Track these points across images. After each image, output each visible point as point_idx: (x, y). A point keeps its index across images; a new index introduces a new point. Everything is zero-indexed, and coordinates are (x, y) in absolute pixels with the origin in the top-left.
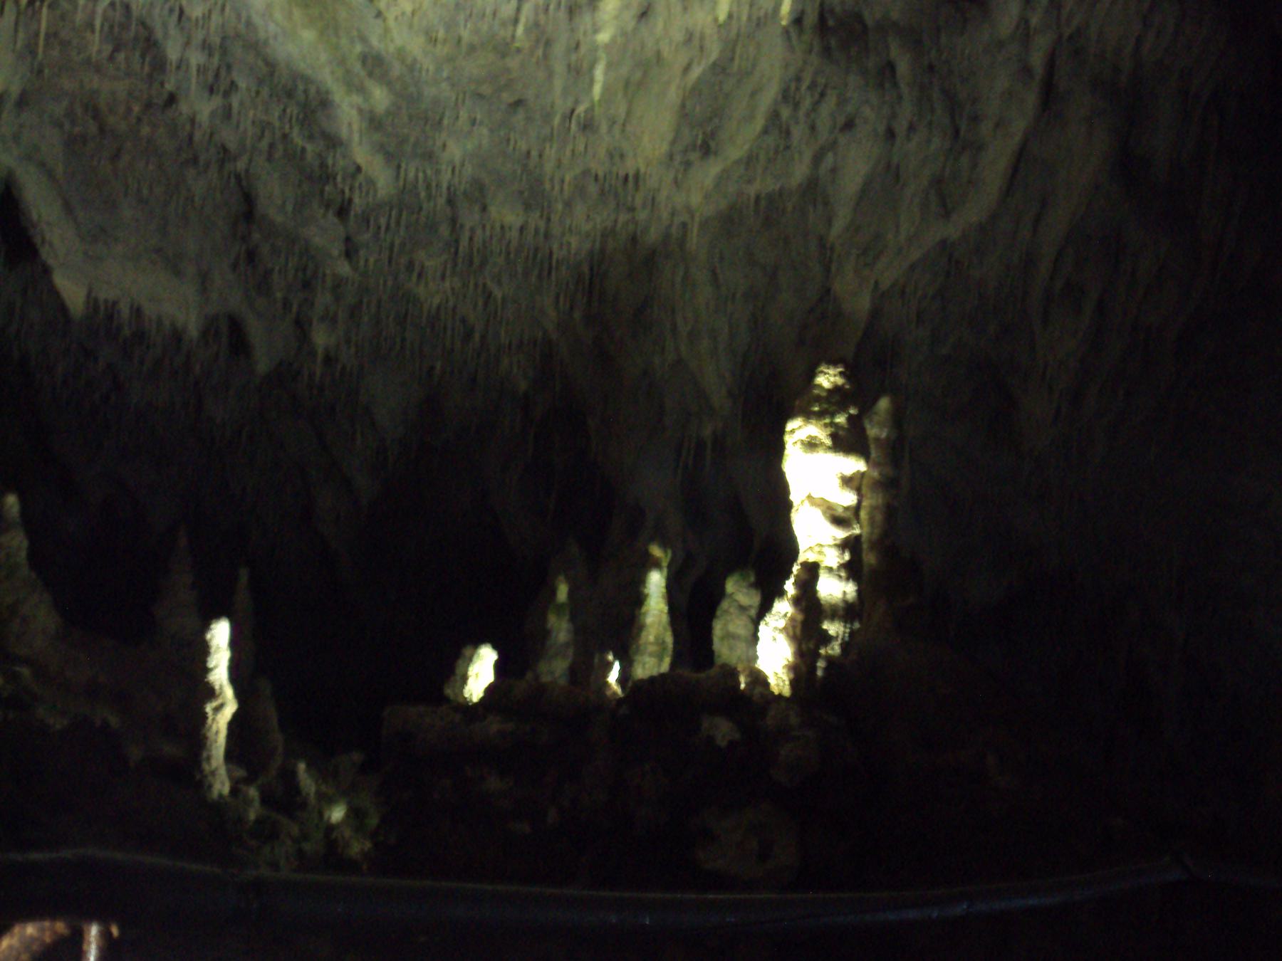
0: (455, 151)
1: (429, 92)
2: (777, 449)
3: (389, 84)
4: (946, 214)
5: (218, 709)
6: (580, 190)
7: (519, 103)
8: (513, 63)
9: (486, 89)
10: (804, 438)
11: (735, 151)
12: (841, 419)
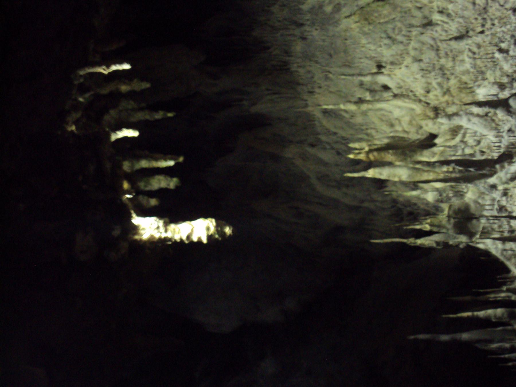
0: (315, 33)
1: (331, 28)
2: (206, 217)
3: (331, 13)
4: (319, 179)
5: (104, 70)
6: (309, 72)
7: (331, 56)
8: (342, 54)
9: (333, 46)
10: (210, 227)
11: (325, 122)
12: (217, 236)
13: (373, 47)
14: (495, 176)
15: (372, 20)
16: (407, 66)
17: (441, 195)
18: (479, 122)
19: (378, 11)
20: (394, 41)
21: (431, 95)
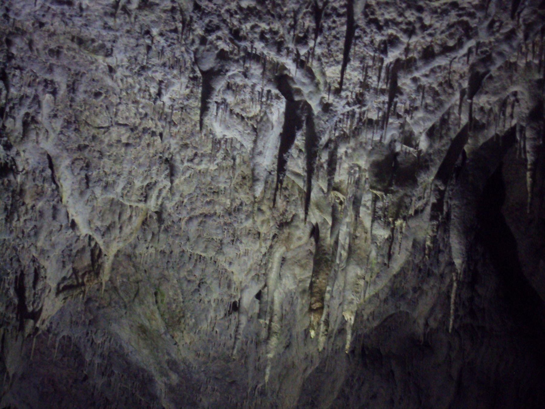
7: (233, 383)
8: (231, 365)
13: (212, 314)
14: (310, 102)
15: (180, 312)
16: (230, 263)
17: (380, 218)
18: (262, 140)
19: (169, 303)
20: (201, 283)
21: (263, 230)
